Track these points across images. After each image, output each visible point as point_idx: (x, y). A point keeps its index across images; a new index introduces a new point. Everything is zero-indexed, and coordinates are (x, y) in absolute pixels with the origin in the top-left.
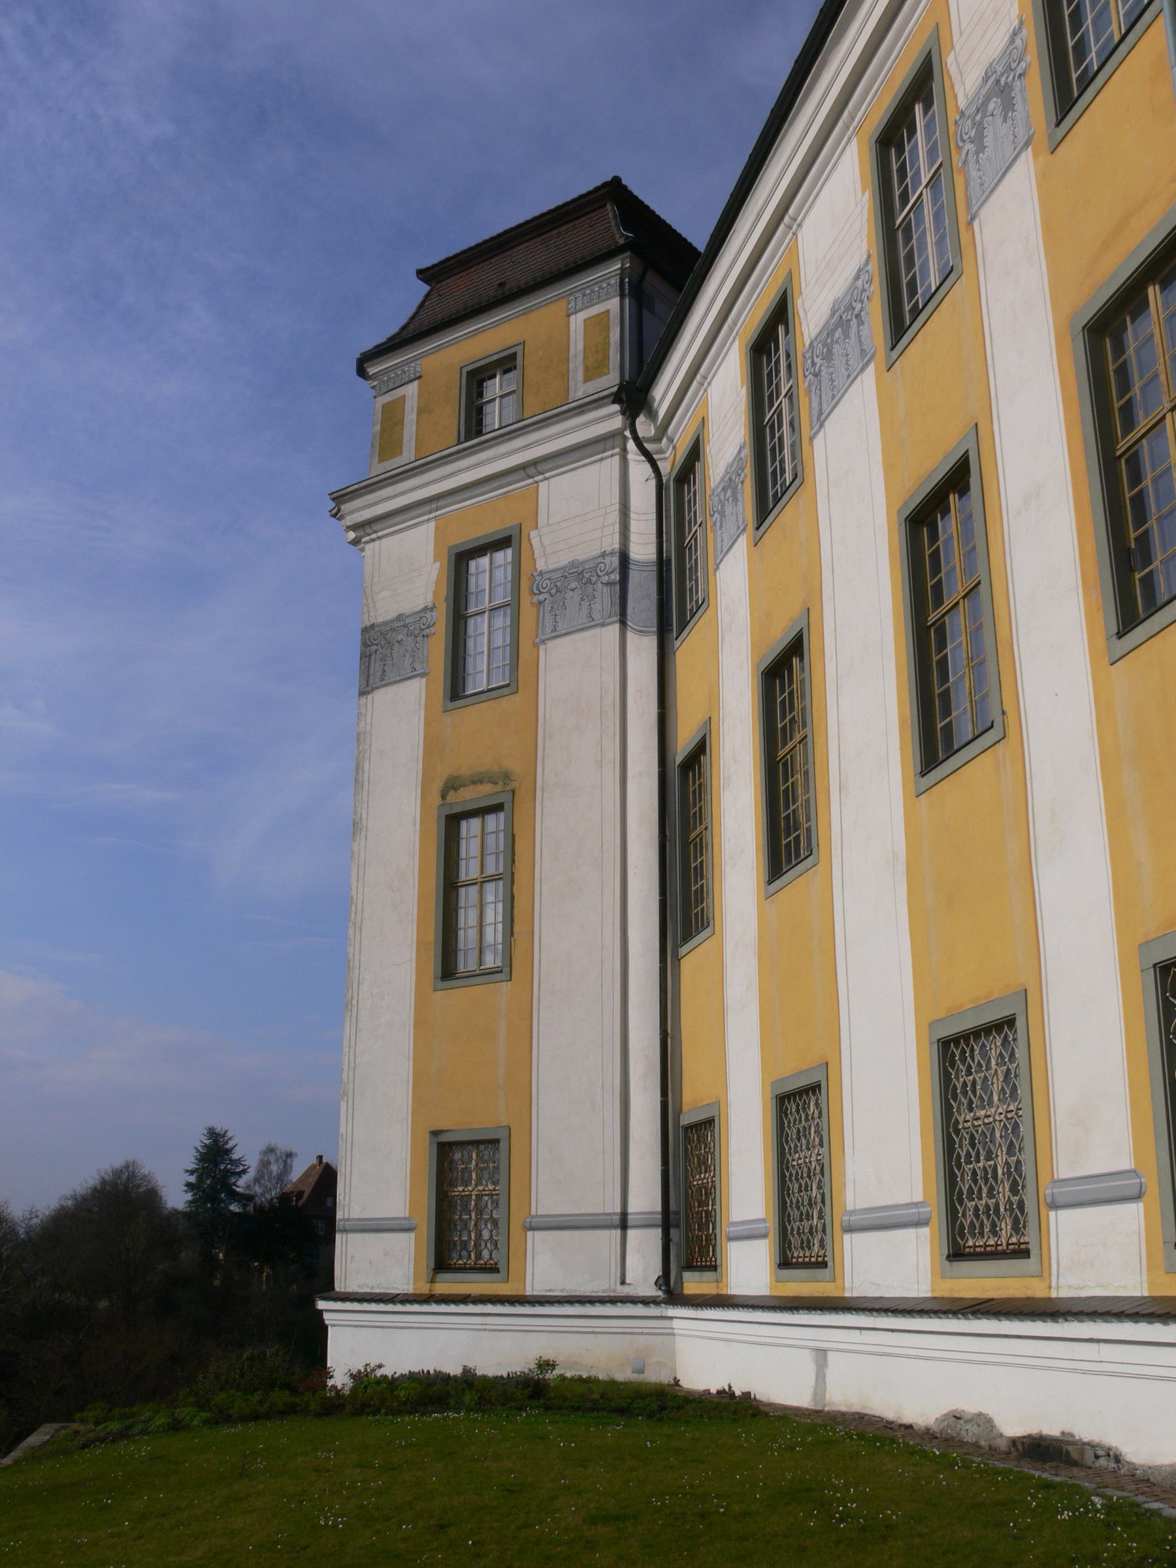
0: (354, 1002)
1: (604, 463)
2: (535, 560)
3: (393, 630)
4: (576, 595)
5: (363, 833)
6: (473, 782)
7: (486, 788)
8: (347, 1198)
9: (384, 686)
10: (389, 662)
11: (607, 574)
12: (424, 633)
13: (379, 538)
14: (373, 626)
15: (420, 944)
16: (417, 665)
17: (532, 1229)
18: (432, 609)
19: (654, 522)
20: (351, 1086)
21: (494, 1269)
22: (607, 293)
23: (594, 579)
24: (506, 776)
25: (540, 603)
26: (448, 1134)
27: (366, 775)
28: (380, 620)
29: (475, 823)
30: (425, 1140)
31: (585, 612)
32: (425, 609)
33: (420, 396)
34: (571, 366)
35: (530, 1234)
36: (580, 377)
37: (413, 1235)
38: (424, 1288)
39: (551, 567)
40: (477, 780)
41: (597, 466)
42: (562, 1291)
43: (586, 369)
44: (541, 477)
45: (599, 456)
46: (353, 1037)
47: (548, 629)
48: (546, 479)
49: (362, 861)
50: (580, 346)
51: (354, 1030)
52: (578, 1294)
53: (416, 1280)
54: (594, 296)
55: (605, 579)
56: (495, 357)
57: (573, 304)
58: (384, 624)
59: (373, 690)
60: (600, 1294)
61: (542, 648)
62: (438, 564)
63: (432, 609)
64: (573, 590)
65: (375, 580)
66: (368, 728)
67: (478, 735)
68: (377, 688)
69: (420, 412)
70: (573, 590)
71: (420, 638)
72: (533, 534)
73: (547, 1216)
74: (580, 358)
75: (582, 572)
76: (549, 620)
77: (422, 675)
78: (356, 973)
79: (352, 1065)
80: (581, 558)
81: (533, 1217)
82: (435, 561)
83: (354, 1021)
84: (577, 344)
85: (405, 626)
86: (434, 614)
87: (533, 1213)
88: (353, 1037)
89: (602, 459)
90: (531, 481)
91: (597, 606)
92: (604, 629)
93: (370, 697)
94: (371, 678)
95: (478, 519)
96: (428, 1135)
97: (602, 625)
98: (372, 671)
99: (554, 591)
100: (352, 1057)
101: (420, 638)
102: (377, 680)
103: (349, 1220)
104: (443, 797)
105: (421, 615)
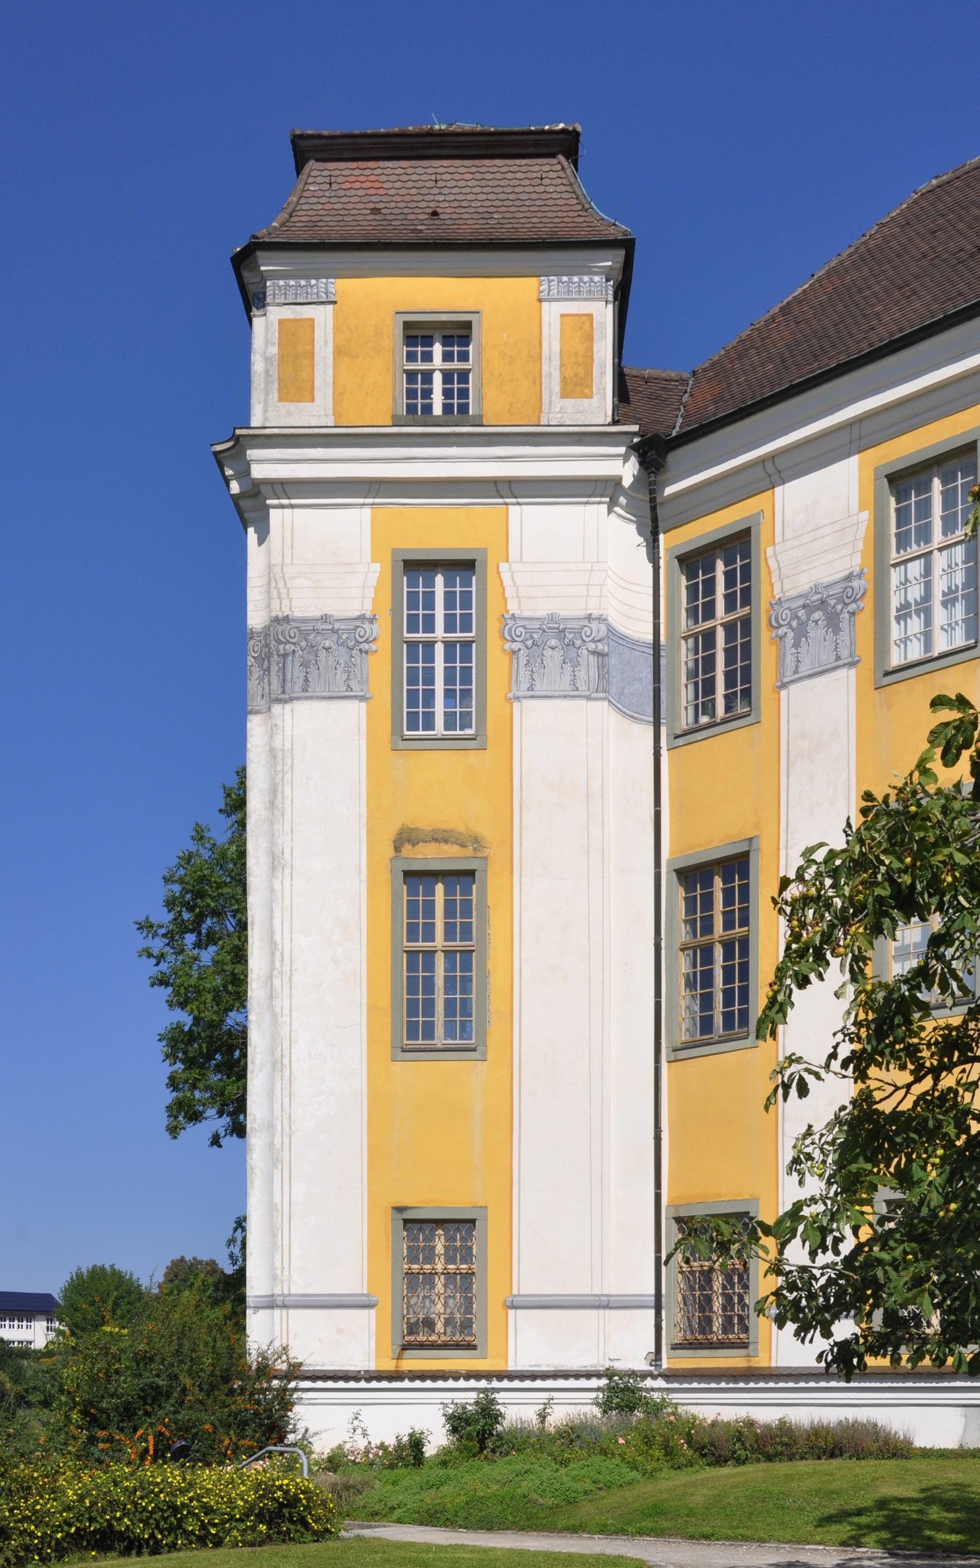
0: (286, 1062)
1: (588, 507)
2: (505, 599)
3: (317, 632)
4: (558, 654)
5: (287, 871)
6: (436, 840)
7: (452, 850)
8: (286, 1272)
9: (307, 698)
10: (312, 669)
11: (594, 641)
12: (362, 646)
13: (292, 506)
14: (287, 619)
15: (372, 1009)
16: (353, 684)
17: (513, 1307)
18: (372, 620)
19: (651, 598)
20: (286, 1154)
21: (470, 1347)
22: (589, 291)
23: (578, 643)
24: (477, 841)
25: (514, 652)
26: (415, 1210)
27: (288, 802)
28: (298, 614)
29: (941, 645)
30: (386, 1218)
31: (567, 678)
32: (362, 618)
33: (337, 329)
34: (545, 368)
35: (511, 1312)
36: (557, 389)
37: (373, 1312)
38: (389, 1365)
39: (526, 614)
40: (440, 837)
41: (581, 507)
42: (548, 1366)
43: (564, 380)
44: (514, 500)
45: (586, 500)
46: (286, 1101)
47: (524, 685)
48: (519, 504)
49: (287, 902)
50: (556, 347)
51: (286, 1093)
52: (564, 1368)
53: (378, 1356)
54: (574, 288)
55: (592, 646)
56: (443, 318)
57: (545, 287)
58: (305, 620)
59: (291, 699)
60: (589, 1368)
61: (516, 705)
62: (377, 567)
63: (372, 620)
64: (553, 648)
65: (288, 560)
66: (288, 745)
67: (440, 787)
68: (298, 699)
69: (339, 352)
70: (553, 648)
71: (355, 652)
72: (503, 567)
73: (530, 1296)
74: (556, 362)
75: (563, 631)
76: (524, 675)
77: (362, 698)
78: (287, 1029)
79: (287, 1128)
80: (564, 613)
81: (515, 1296)
82: (374, 560)
83: (286, 1081)
84: (552, 345)
85: (334, 631)
86: (375, 627)
87: (515, 1292)
88: (286, 1101)
89: (587, 503)
90: (500, 500)
91: (582, 674)
92: (591, 703)
93: (288, 707)
94: (288, 685)
95: (440, 528)
96: (390, 1210)
97: (589, 698)
98: (289, 676)
99: (529, 643)
100: (286, 1122)
101: (355, 652)
102: (298, 688)
103: (289, 1295)
104: (397, 849)
105: (358, 623)
